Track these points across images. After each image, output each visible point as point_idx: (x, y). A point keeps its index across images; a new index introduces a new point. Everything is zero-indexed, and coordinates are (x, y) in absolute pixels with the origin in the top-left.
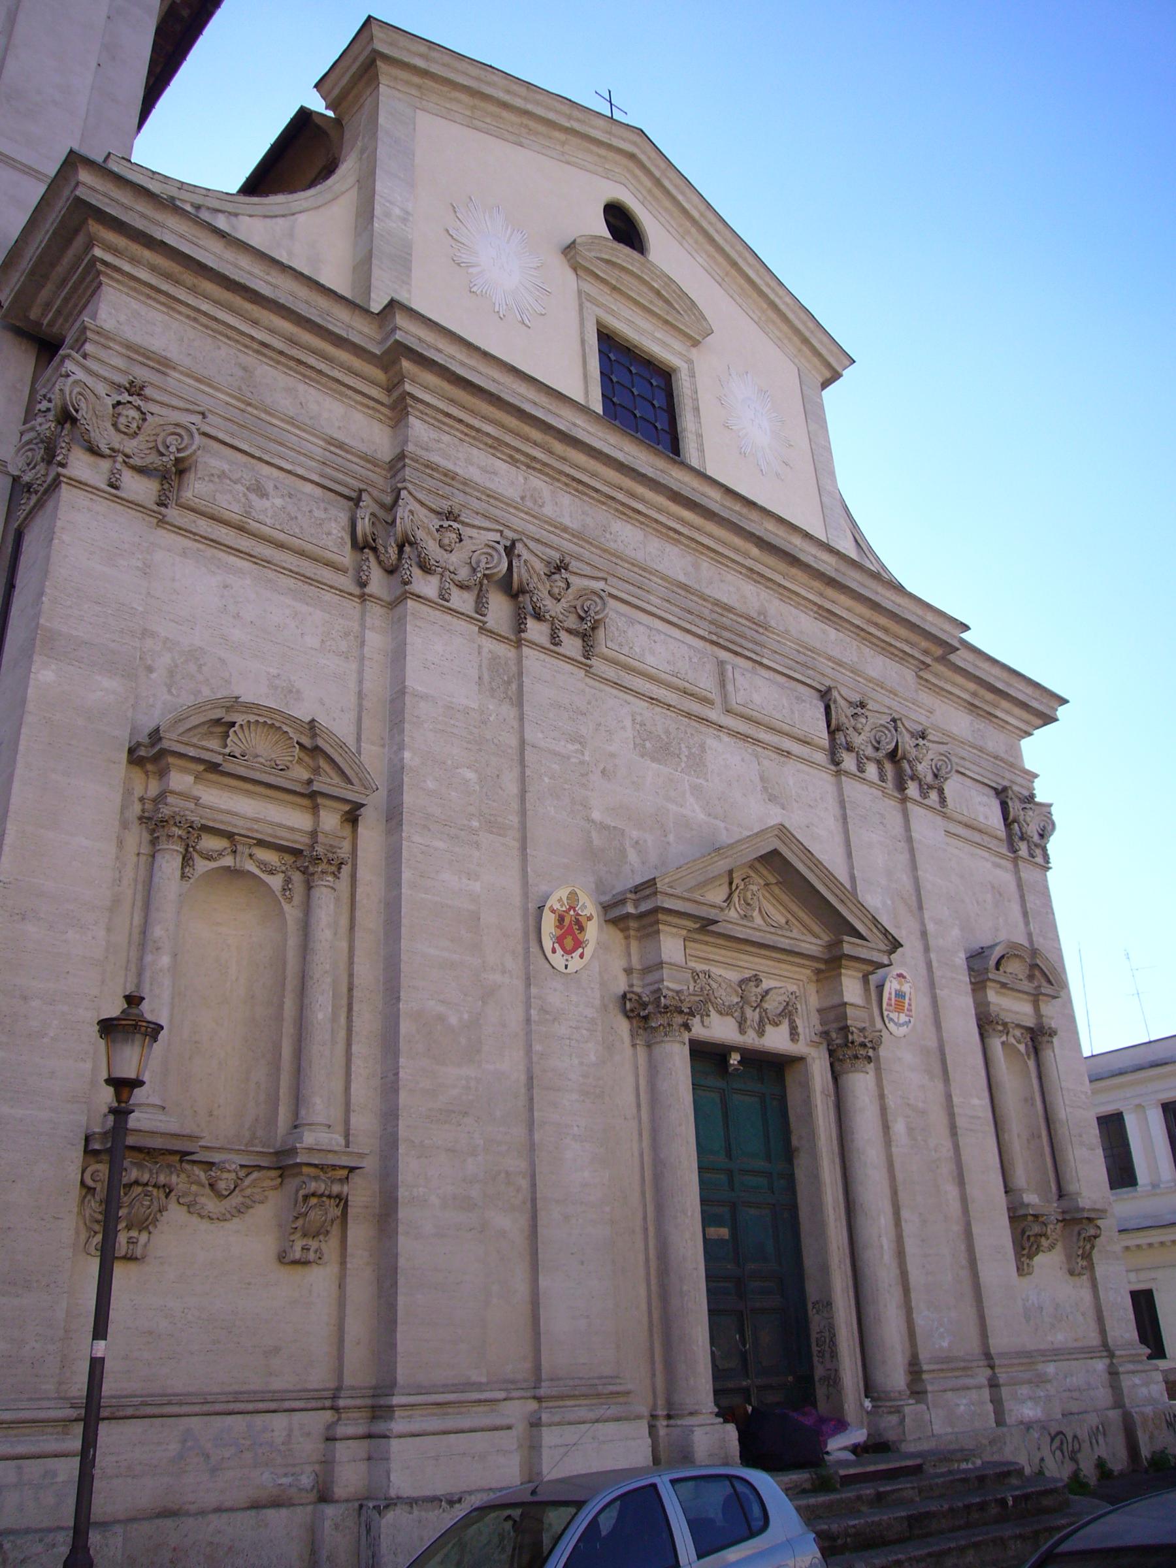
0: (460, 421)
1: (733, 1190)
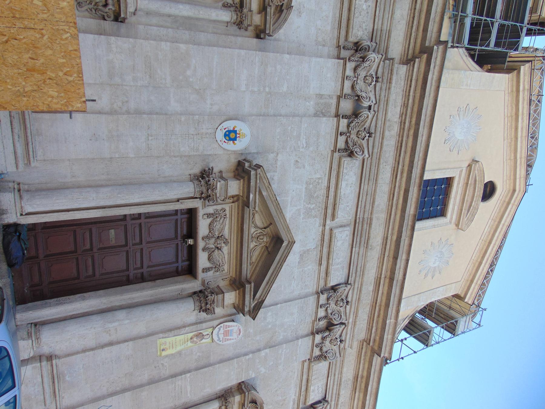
0: (410, 86)
1: (133, 245)
